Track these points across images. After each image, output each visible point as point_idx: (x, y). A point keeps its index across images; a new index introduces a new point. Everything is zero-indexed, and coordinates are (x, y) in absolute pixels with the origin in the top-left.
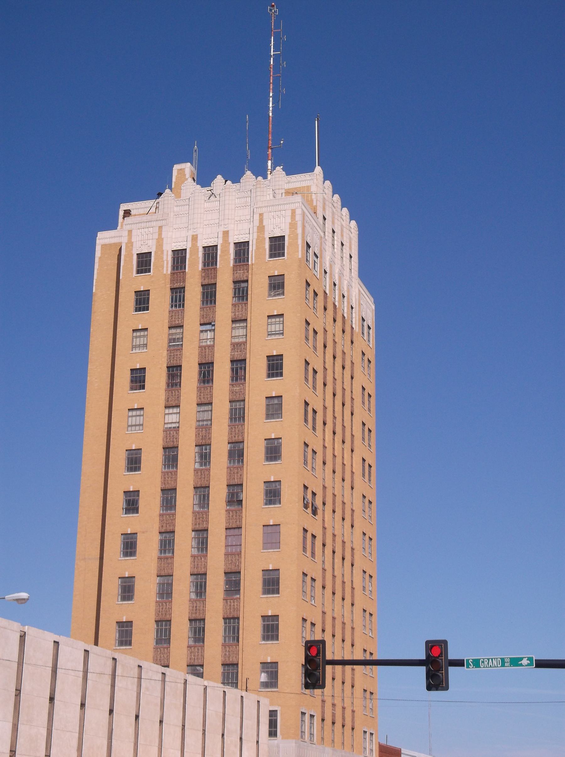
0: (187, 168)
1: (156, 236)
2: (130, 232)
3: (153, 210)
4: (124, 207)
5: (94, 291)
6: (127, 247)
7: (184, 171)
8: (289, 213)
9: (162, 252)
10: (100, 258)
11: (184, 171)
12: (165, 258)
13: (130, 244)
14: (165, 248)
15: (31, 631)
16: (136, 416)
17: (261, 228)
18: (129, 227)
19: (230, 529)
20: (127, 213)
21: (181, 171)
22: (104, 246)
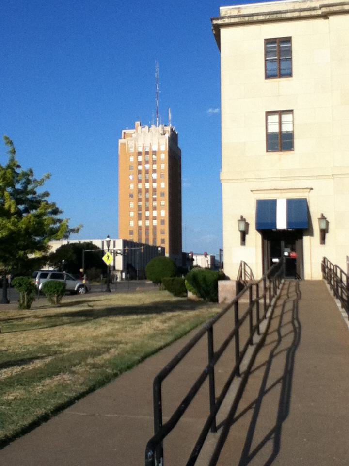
4: (123, 131)
20: (125, 133)
22: (122, 144)
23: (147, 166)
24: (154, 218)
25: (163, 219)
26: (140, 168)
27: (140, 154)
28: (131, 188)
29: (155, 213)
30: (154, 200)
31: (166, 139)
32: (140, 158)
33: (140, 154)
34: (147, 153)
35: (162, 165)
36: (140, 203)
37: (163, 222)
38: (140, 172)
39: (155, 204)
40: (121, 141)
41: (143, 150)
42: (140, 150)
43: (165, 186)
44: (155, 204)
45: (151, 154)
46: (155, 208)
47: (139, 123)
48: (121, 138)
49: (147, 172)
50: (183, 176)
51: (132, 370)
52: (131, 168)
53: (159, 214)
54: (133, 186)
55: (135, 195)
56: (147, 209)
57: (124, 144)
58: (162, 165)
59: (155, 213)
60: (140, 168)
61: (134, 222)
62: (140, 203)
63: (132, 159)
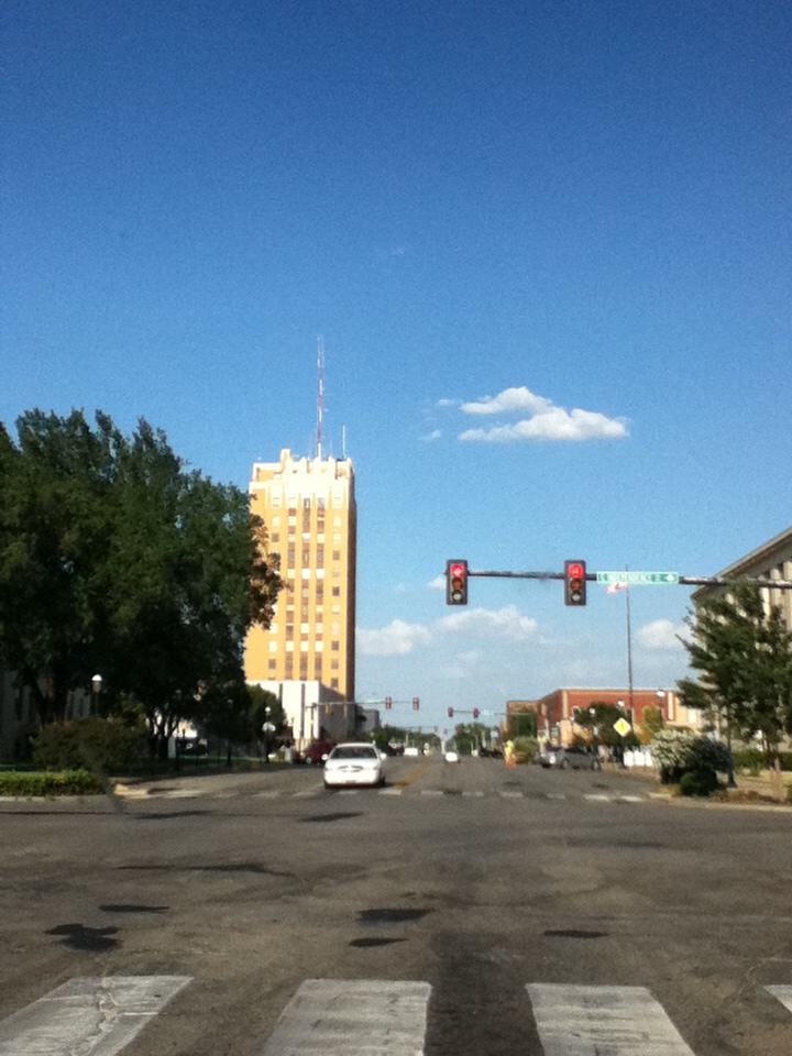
4: (256, 466)
7: (285, 452)
20: (258, 470)
29: (320, 628)
36: (291, 608)
37: (335, 646)
47: (288, 451)
48: (251, 480)
56: (305, 619)
59: (320, 628)
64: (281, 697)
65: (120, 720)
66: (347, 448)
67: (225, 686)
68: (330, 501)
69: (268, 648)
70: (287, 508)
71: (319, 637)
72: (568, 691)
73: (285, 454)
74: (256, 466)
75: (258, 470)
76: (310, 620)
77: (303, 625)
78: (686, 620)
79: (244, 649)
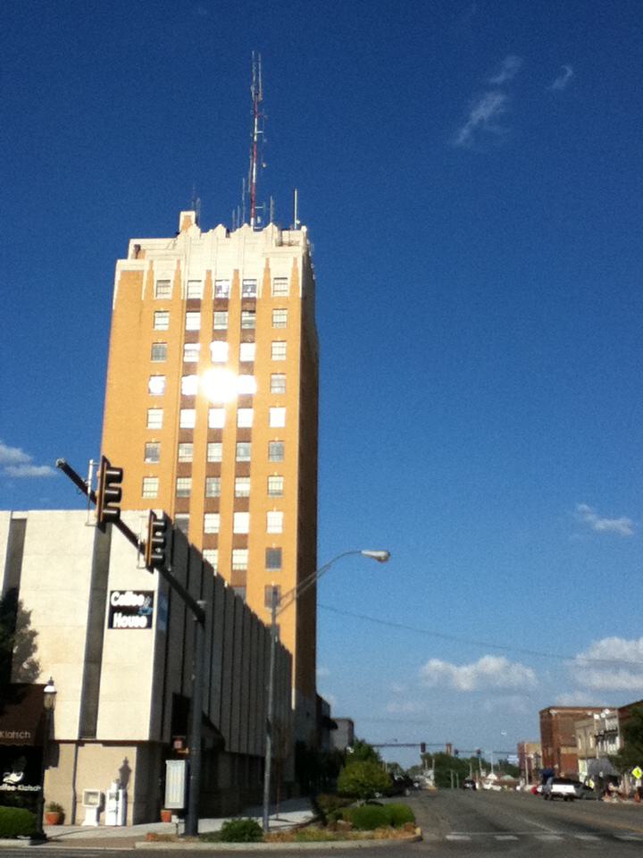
0: (192, 214)
1: (175, 267)
2: (152, 262)
3: (171, 245)
4: (133, 242)
5: (114, 308)
6: (148, 274)
7: (187, 217)
8: (175, 262)
9: (180, 280)
10: (119, 282)
11: (187, 217)
12: (182, 287)
13: (151, 272)
14: (182, 278)
15: (95, 824)
16: (276, 482)
17: (267, 270)
18: (150, 258)
19: (189, 553)
20: (138, 248)
21: (188, 218)
22: (124, 273)
23: (216, 453)
24: (241, 542)
25: (274, 546)
26: (186, 454)
27: (194, 305)
28: (151, 426)
29: (242, 523)
30: (243, 470)
31: (295, 259)
32: (194, 321)
33: (194, 305)
34: (221, 305)
35: (270, 515)
36: (184, 484)
37: (274, 559)
38: (184, 470)
39: (243, 486)
40: (122, 265)
41: (207, 292)
42: (197, 292)
43: (287, 420)
44: (243, 486)
45: (235, 306)
46: (242, 504)
47: (192, 214)
48: (125, 256)
49: (214, 470)
50: (319, 665)
51: (60, 804)
52: (156, 353)
53: (260, 523)
54: (156, 487)
55: (166, 450)
56: (212, 506)
57: (137, 275)
58: (270, 515)
59: (242, 523)
60: (186, 454)
61: (160, 485)
62: (184, 484)
63: (162, 323)
64: (220, 727)
65: (363, 801)
66: (274, 216)
67: (590, 518)
68: (267, 281)
69: (276, 535)
70: (184, 297)
71: (241, 542)
72: (42, 790)
73: (188, 218)
74: (133, 242)
75: (138, 248)
76: (222, 508)
77: (238, 516)
78: (51, 683)
79: (34, 634)
